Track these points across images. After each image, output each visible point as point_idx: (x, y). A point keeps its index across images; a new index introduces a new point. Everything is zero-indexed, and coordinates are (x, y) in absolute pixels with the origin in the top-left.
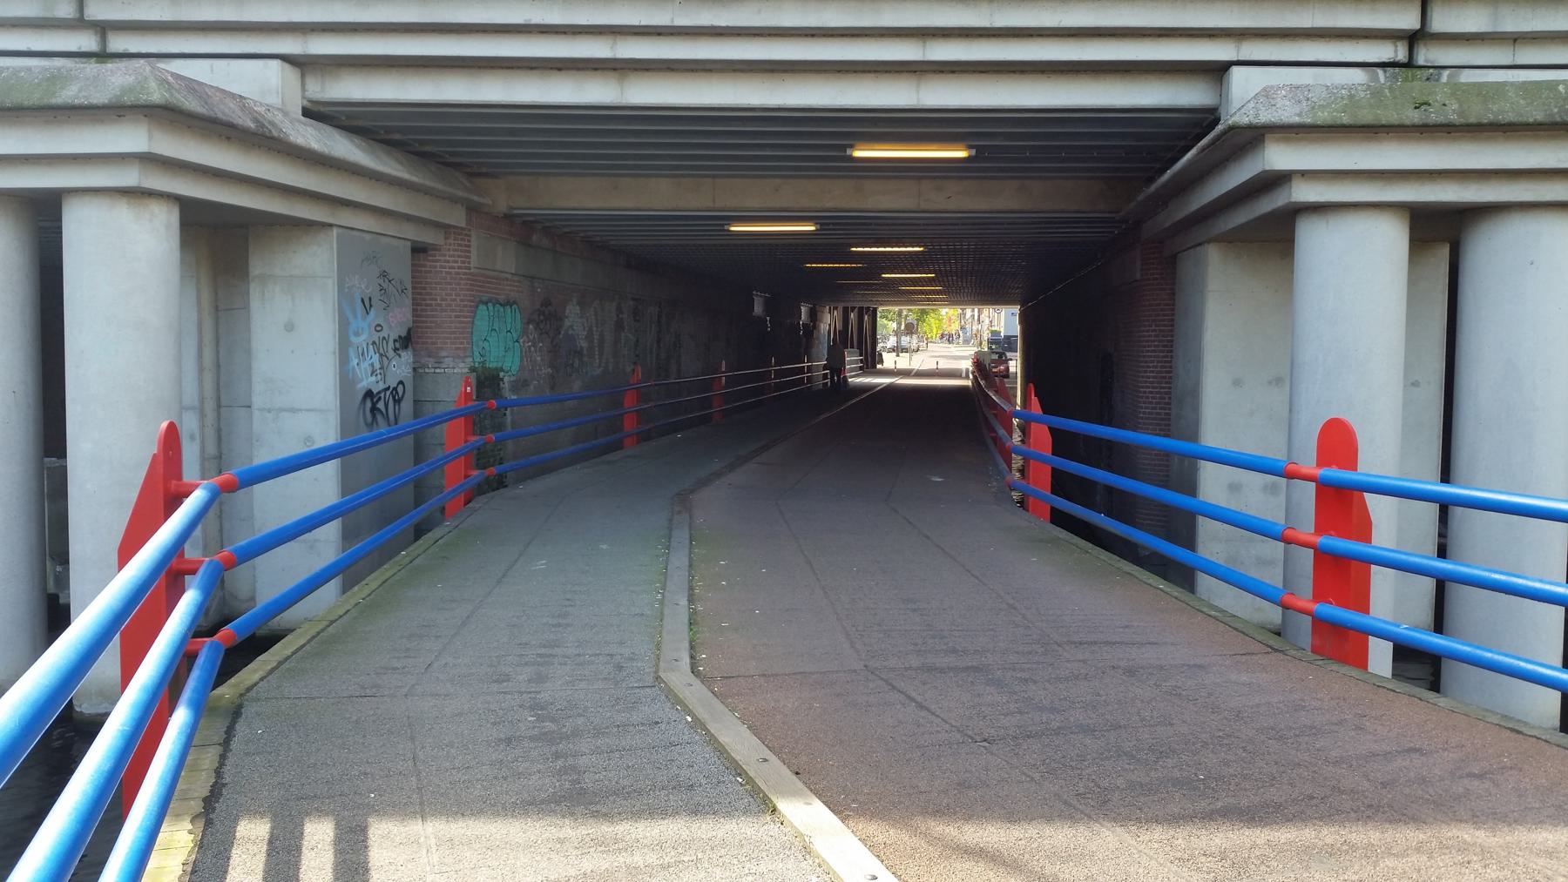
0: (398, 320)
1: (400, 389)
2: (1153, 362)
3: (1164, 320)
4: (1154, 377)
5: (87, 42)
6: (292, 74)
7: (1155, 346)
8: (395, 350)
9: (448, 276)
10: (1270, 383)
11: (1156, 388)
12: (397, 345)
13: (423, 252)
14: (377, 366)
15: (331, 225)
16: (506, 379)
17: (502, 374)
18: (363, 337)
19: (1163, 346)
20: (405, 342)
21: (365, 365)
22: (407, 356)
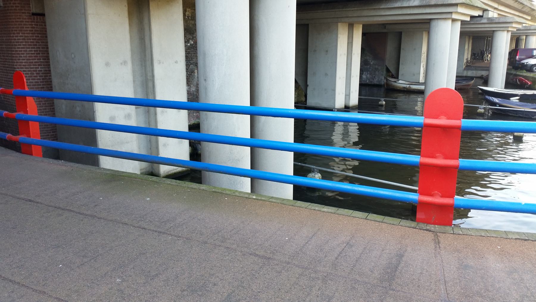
2: (24, 54)
3: (27, 31)
4: (25, 62)
7: (23, 45)
9: (35, 73)
10: (122, 64)
11: (28, 68)
13: (459, 89)
19: (29, 45)
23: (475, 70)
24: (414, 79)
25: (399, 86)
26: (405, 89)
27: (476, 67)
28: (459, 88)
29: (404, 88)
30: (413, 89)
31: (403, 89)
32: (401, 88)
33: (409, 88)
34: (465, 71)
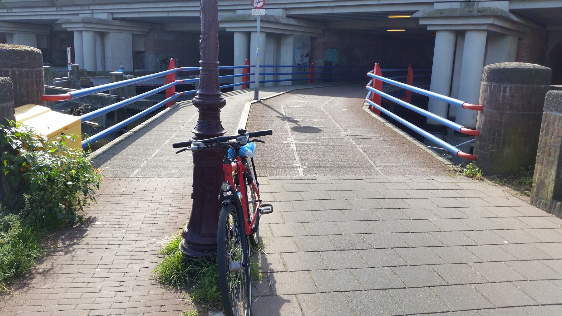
0: (307, 51)
1: (306, 64)
5: (91, 12)
6: (284, 11)
8: (305, 57)
12: (306, 56)
14: (301, 59)
15: (292, 35)
16: (333, 64)
17: (332, 63)
18: (299, 54)
20: (307, 55)
21: (298, 59)
22: (308, 58)
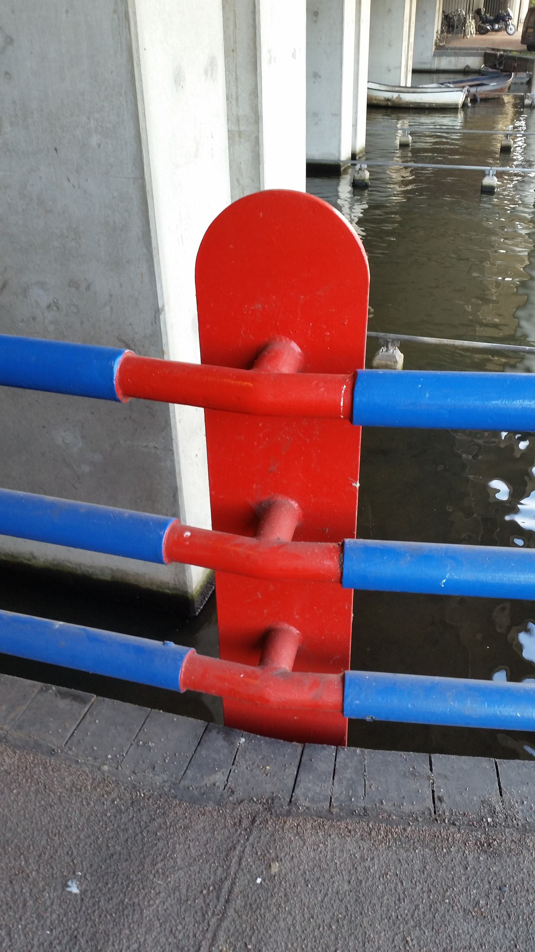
23: (453, 56)
24: (390, 79)
25: (376, 97)
26: (390, 103)
27: (455, 49)
28: (484, 96)
29: (388, 100)
30: (407, 102)
31: (384, 103)
32: (382, 100)
33: (397, 100)
34: (436, 58)
